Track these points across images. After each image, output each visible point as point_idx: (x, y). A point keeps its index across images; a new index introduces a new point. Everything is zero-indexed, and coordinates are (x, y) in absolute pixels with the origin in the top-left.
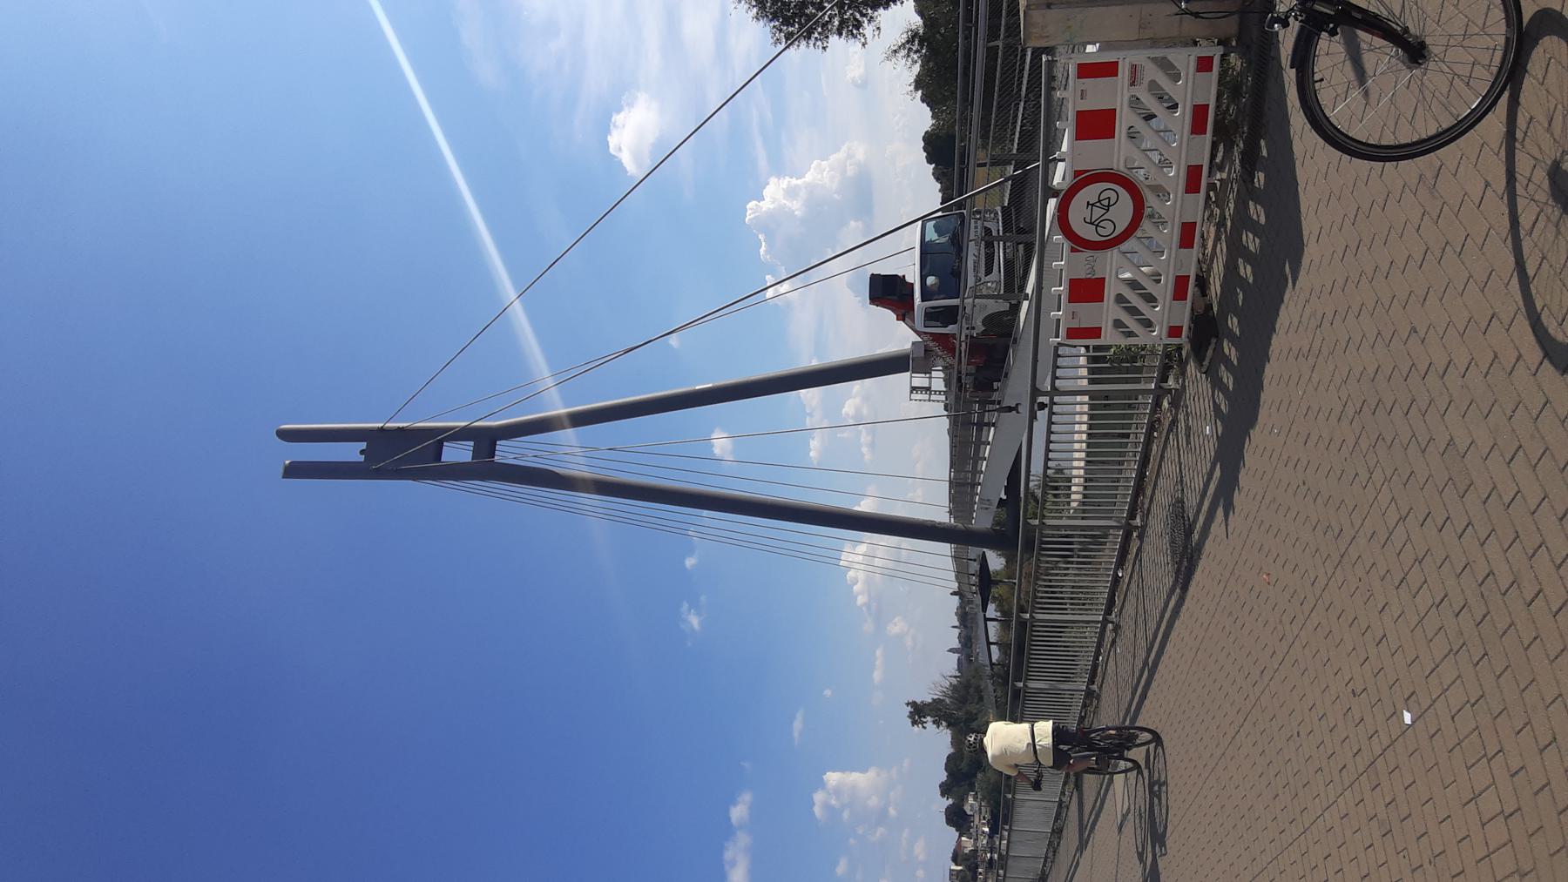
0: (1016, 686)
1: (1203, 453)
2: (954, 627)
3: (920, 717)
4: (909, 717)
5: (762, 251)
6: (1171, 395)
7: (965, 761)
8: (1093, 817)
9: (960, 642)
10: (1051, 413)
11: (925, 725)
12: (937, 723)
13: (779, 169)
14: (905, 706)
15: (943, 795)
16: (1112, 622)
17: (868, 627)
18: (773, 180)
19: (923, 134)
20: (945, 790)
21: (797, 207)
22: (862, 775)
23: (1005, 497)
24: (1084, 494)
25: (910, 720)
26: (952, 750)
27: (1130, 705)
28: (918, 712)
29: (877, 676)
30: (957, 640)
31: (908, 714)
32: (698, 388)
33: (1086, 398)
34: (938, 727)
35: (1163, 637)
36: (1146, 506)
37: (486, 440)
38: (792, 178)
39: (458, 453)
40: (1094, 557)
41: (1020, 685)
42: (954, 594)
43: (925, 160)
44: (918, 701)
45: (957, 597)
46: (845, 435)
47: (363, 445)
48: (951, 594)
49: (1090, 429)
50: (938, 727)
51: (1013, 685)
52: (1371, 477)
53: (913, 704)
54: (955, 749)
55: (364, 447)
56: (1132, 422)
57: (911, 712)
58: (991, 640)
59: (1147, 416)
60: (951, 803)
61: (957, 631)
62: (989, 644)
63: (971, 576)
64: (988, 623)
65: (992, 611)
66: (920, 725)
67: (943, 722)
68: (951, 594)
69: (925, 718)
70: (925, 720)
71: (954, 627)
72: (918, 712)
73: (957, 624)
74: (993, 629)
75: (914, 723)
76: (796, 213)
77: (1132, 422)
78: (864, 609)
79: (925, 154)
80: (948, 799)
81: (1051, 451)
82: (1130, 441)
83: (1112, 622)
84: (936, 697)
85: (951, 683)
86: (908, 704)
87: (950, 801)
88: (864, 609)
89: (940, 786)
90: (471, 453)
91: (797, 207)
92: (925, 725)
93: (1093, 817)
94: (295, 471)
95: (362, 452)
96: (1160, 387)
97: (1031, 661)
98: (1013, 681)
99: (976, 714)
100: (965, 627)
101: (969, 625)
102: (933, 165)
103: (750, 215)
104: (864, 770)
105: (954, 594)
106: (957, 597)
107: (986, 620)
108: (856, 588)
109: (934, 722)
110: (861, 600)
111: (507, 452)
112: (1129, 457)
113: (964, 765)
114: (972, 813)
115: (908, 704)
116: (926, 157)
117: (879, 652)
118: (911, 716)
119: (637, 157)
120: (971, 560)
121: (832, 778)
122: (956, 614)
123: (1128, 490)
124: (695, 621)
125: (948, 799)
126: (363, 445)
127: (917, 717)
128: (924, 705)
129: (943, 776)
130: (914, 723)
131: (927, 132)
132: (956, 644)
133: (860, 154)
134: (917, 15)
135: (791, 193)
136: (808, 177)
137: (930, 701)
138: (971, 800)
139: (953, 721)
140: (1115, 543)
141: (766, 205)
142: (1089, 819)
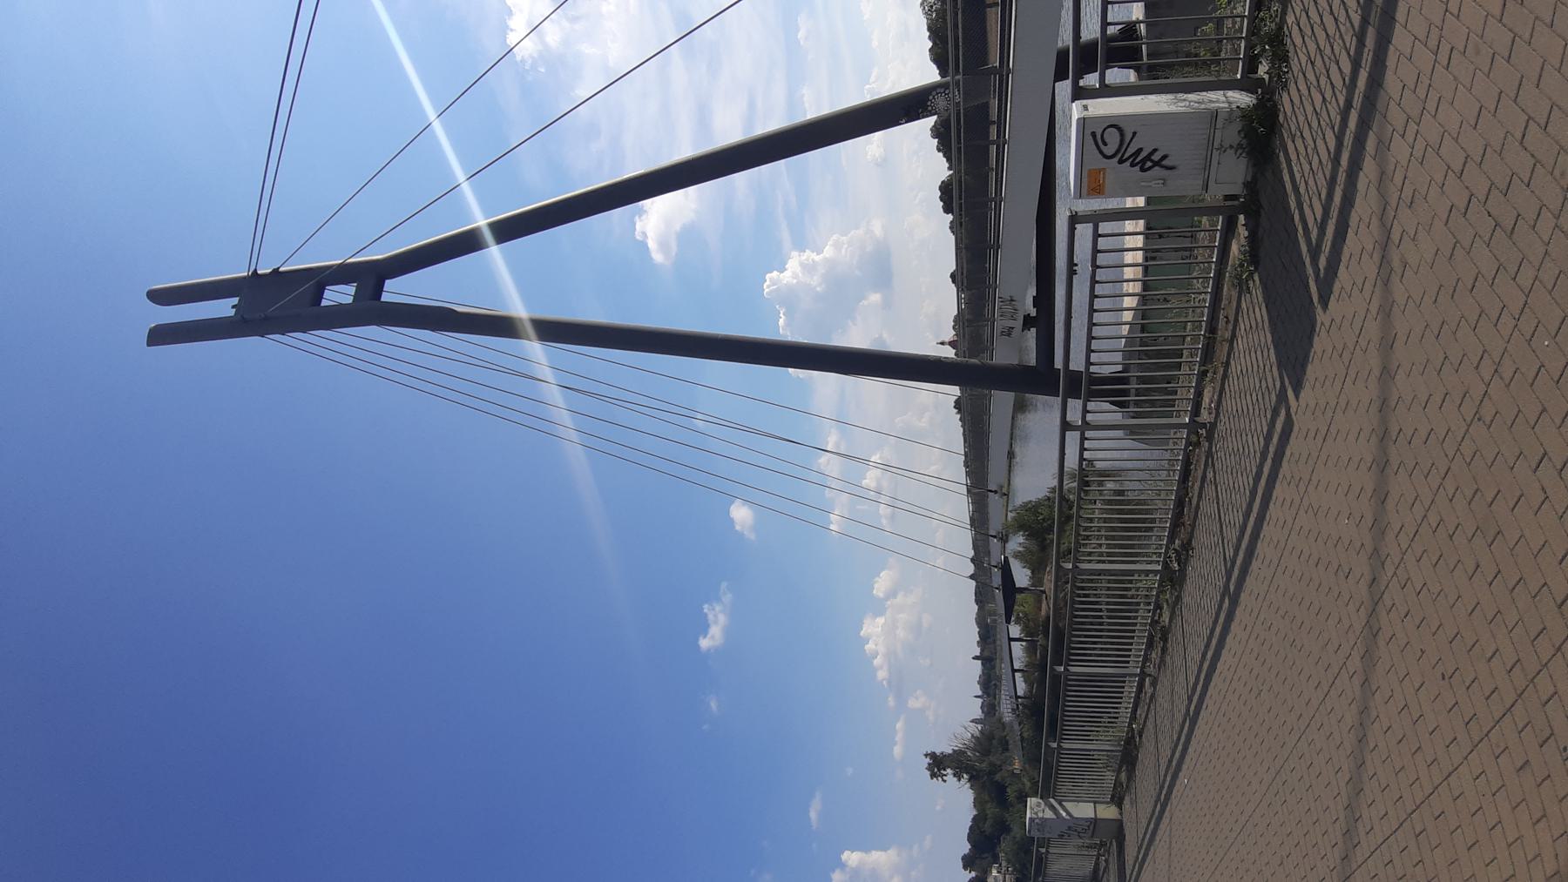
0: (1055, 670)
1: (1216, 575)
2: (976, 697)
3: (939, 770)
4: (928, 769)
5: (781, 322)
6: (1206, 428)
7: (988, 823)
8: (1152, 826)
9: (983, 712)
10: (1083, 439)
11: (945, 778)
12: (958, 776)
13: (801, 246)
14: (924, 757)
15: (965, 867)
16: (1150, 675)
17: (891, 702)
18: (795, 254)
19: (940, 183)
20: (968, 862)
21: (815, 281)
22: (883, 853)
23: (1033, 313)
24: (1144, 296)
25: (929, 773)
26: (975, 813)
27: (1170, 761)
28: (938, 764)
29: (897, 751)
30: (980, 711)
31: (926, 765)
32: (625, 177)
33: (1140, 225)
34: (959, 780)
35: (1250, 541)
36: (1194, 501)
37: (372, 276)
38: (813, 252)
39: (339, 295)
40: (1140, 546)
41: (1055, 745)
42: (976, 658)
43: (942, 210)
44: (938, 752)
45: (979, 662)
46: (866, 507)
48: (973, 658)
49: (1144, 290)
50: (959, 780)
51: (1052, 670)
52: (1403, 558)
53: (933, 756)
54: (978, 810)
55: (236, 302)
56: (1173, 409)
57: (929, 764)
58: (1016, 667)
59: (1174, 492)
60: (974, 875)
61: (980, 701)
62: (1014, 671)
63: (991, 538)
64: (1012, 643)
65: (1015, 630)
66: (940, 778)
67: (965, 775)
68: (973, 658)
69: (945, 770)
70: (945, 773)
71: (976, 697)
72: (938, 764)
73: (980, 693)
74: (1018, 649)
75: (933, 775)
76: (818, 289)
77: (1173, 409)
78: (885, 682)
79: (942, 204)
80: (970, 872)
81: (1086, 450)
82: (1185, 346)
83: (1150, 675)
84: (956, 748)
85: (972, 735)
86: (926, 755)
87: (973, 874)
88: (885, 682)
89: (962, 859)
90: (352, 298)
91: (815, 281)
92: (945, 778)
93: (1152, 826)
96: (1194, 421)
97: (1060, 772)
98: (1046, 742)
99: (1000, 766)
100: (988, 695)
101: (992, 692)
102: (973, 874)
103: (768, 287)
104: (885, 849)
105: (976, 658)
106: (979, 662)
107: (1014, 671)
108: (877, 662)
109: (955, 775)
110: (882, 674)
111: (397, 290)
112: (1185, 370)
113: (987, 827)
115: (926, 755)
116: (939, 74)
117: (899, 725)
118: (930, 768)
119: (663, 246)
120: (991, 491)
121: (852, 858)
122: (979, 683)
123: (1161, 549)
124: (713, 705)
125: (970, 872)
127: (936, 770)
128: (944, 756)
129: (966, 848)
130: (933, 775)
131: (943, 182)
132: (978, 714)
133: (877, 228)
134: (932, 63)
135: (809, 268)
136: (828, 252)
137: (951, 752)
138: (994, 873)
139: (974, 773)
140: (1129, 703)
141: (787, 277)
142: (1133, 871)
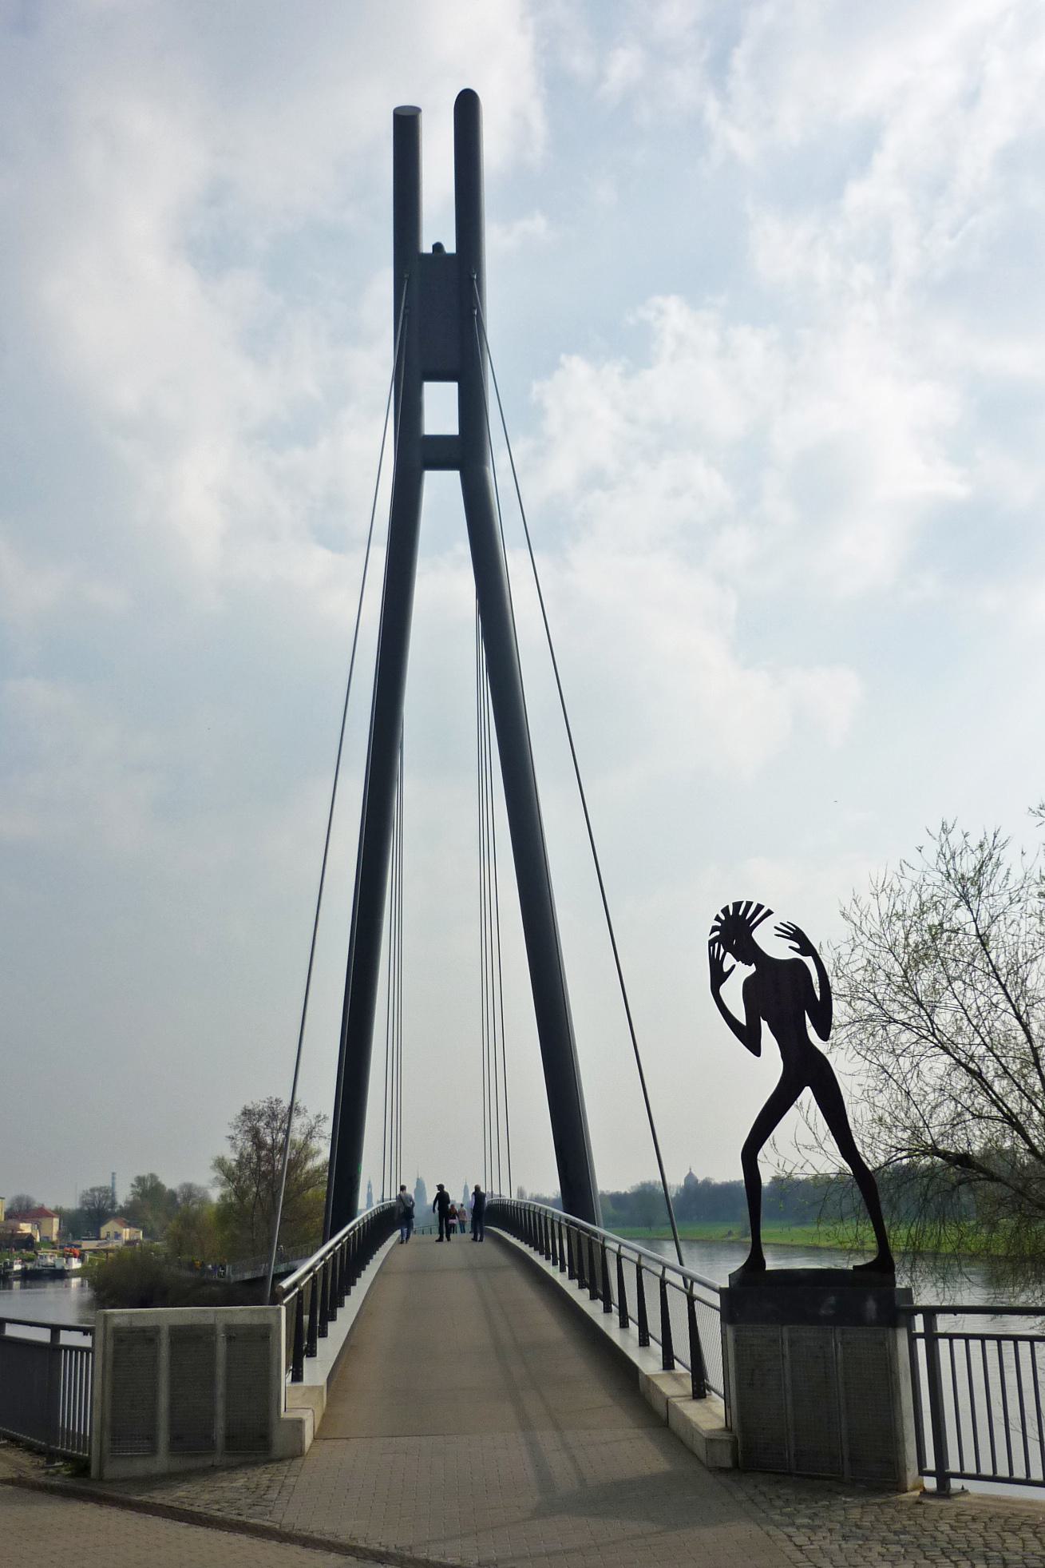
15: (141, 1180)
47: (450, 247)
94: (406, 125)
95: (438, 247)
114: (103, 1234)
126: (450, 247)
